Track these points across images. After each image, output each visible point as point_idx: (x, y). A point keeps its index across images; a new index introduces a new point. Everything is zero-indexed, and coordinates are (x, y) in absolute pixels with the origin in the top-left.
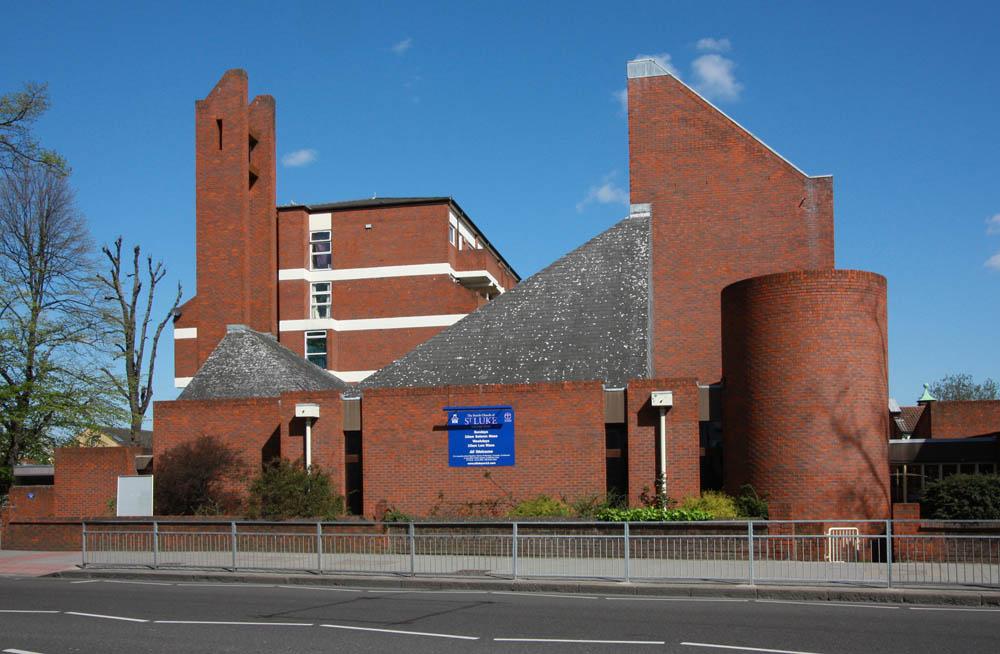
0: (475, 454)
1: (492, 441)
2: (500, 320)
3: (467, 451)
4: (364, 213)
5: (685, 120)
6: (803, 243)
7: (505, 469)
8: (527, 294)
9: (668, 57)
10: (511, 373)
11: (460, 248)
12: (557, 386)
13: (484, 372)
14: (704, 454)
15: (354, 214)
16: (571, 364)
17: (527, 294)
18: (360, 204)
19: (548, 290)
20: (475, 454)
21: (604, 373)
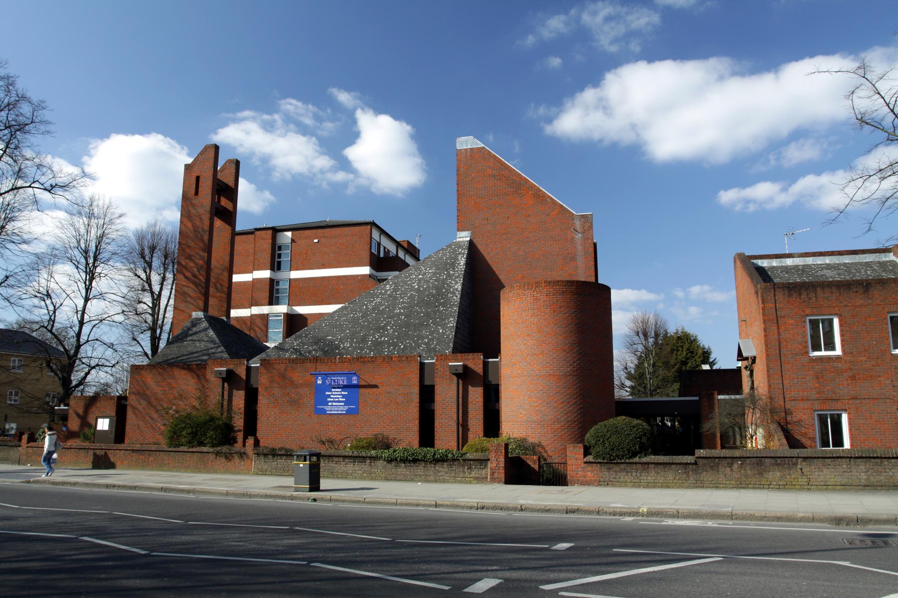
1: (344, 396)
2: (361, 311)
3: (326, 404)
4: (313, 231)
5: (494, 176)
6: (573, 259)
9: (408, 128)
10: (362, 349)
11: (382, 255)
15: (307, 232)
17: (380, 294)
19: (395, 290)
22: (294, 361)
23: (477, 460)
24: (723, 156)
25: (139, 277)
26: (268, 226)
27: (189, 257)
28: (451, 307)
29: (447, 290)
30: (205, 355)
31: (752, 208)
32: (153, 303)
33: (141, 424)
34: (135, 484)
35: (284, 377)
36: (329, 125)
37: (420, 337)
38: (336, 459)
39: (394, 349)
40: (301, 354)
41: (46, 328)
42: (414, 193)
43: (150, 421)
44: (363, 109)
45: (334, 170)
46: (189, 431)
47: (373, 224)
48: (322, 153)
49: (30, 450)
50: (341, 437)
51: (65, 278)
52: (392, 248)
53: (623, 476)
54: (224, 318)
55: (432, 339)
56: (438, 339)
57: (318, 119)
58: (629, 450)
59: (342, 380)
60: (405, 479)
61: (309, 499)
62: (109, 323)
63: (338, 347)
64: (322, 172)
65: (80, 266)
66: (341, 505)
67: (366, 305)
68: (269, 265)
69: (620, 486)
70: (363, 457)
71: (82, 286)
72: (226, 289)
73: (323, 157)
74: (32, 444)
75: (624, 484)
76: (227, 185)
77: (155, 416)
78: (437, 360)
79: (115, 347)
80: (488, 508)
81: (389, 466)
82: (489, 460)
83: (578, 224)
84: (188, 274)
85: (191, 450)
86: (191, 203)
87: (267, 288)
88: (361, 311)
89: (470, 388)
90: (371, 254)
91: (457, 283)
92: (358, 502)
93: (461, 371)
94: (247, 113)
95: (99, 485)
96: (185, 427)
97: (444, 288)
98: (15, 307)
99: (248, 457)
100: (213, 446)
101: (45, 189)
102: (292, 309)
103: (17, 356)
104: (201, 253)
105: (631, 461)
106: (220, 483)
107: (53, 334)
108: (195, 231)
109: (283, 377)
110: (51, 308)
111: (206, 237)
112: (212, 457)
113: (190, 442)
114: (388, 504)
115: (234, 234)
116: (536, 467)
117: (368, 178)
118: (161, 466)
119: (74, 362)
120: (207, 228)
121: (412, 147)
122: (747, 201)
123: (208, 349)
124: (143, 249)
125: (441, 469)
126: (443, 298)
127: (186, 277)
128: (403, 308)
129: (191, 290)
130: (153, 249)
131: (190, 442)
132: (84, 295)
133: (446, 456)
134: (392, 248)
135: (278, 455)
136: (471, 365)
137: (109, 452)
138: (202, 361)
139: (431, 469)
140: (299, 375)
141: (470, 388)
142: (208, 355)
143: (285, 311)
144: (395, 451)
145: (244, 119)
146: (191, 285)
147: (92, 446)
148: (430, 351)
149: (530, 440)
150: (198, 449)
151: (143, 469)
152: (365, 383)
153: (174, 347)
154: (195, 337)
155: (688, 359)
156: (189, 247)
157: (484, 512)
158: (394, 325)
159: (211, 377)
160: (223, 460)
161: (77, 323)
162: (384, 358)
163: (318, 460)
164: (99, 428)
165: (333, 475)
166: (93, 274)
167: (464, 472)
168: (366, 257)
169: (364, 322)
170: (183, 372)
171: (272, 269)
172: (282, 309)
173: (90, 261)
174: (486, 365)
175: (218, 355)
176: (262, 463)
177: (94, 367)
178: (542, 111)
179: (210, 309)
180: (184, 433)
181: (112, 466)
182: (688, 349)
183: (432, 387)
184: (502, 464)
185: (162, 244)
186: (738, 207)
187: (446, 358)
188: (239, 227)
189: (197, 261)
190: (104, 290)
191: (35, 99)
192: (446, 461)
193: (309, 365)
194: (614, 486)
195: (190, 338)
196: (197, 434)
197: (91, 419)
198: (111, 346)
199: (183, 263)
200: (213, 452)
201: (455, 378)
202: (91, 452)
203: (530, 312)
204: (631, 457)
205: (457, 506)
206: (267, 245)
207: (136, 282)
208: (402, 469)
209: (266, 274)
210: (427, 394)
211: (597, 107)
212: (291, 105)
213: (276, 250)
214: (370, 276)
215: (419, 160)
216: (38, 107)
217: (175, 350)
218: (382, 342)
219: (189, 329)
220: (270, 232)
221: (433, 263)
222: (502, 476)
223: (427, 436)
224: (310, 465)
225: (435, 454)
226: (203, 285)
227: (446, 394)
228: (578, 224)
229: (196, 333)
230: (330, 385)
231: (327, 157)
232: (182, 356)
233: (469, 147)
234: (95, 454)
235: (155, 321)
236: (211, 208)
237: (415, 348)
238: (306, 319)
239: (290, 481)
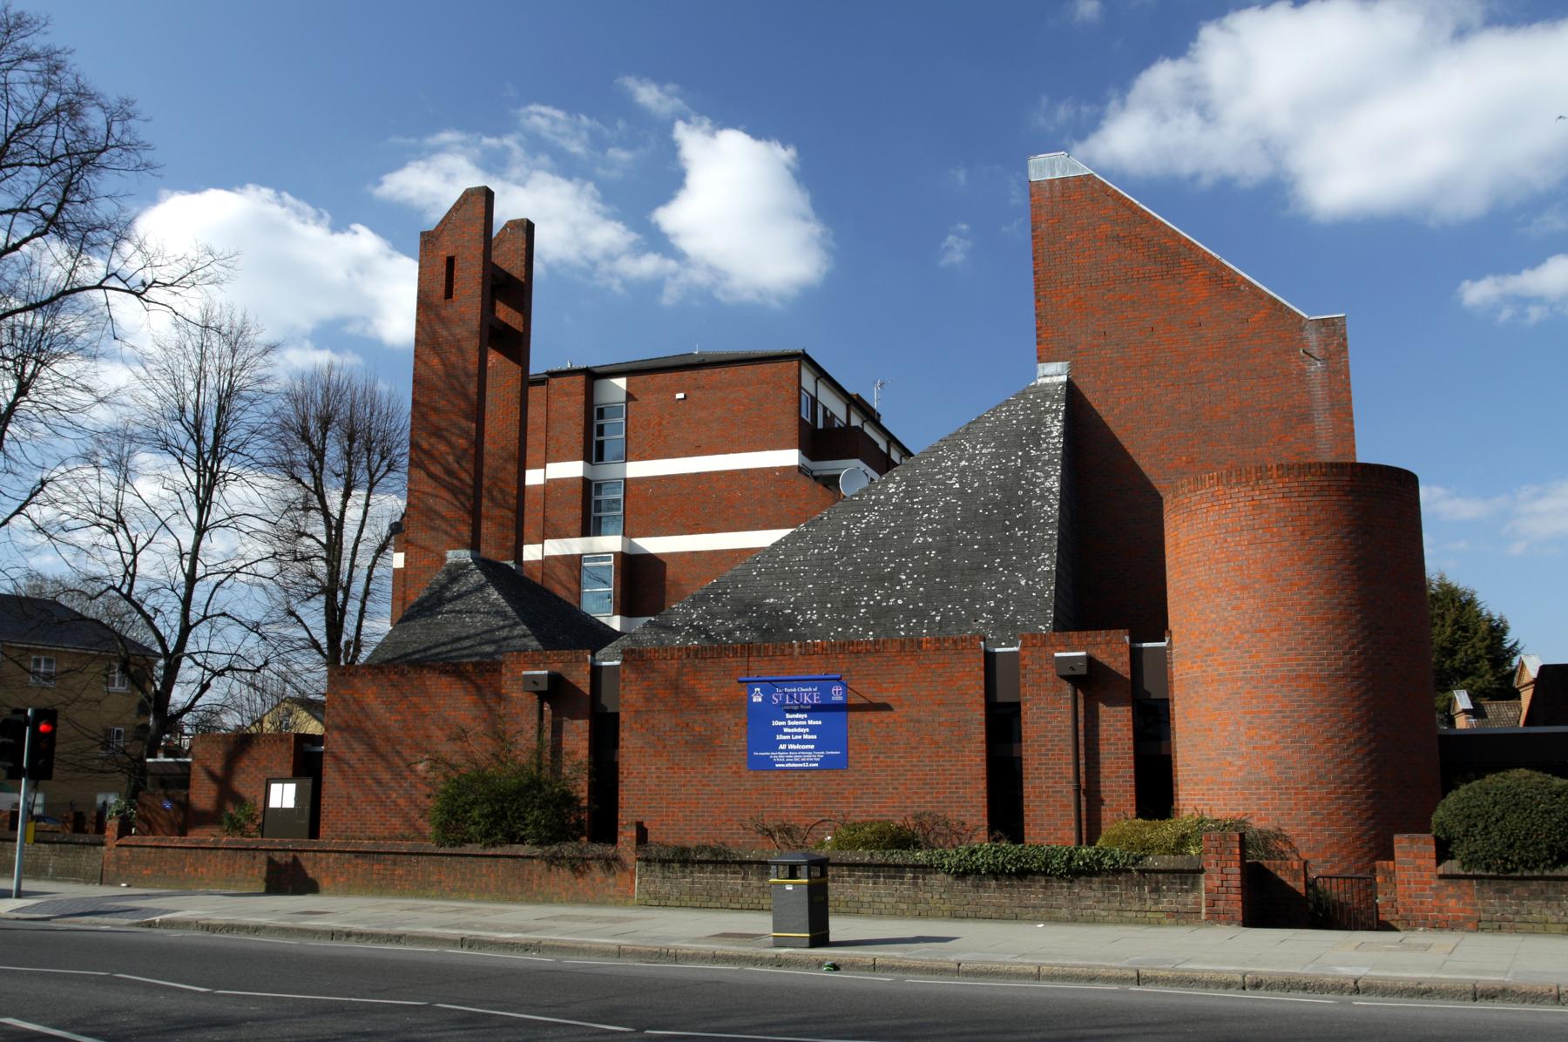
0: (787, 750)
1: (813, 729)
2: (835, 541)
3: (774, 746)
4: (674, 375)
5: (1117, 238)
6: (1305, 417)
10: (847, 624)
11: (820, 425)
12: (913, 645)
13: (805, 623)
14: (1015, 745)
15: (660, 377)
16: (937, 610)
17: (876, 502)
18: (645, 365)
19: (909, 494)
20: (787, 750)
21: (987, 624)
22: (697, 653)
23: (1174, 871)
24: (1470, 203)
25: (299, 481)
26: (576, 366)
27: (437, 433)
28: (1042, 528)
29: (1026, 492)
30: (488, 642)
31: (1535, 313)
32: (329, 536)
33: (356, 794)
34: (401, 929)
35: (677, 688)
36: (621, 155)
37: (977, 596)
39: (920, 623)
40: (709, 637)
41: (119, 590)
42: (808, 299)
43: (376, 788)
44: (687, 121)
45: (638, 250)
46: (487, 809)
47: (803, 358)
48: (608, 217)
49: (126, 852)
50: (809, 820)
51: (158, 483)
52: (838, 408)
53: (1537, 910)
54: (511, 563)
55: (1005, 601)
56: (1017, 601)
57: (599, 143)
58: (1550, 848)
59: (810, 695)
60: (1000, 916)
61: (820, 965)
62: (229, 583)
63: (791, 621)
64: (610, 257)
65: (185, 459)
66: (912, 980)
67: (847, 528)
68: (580, 449)
69: (1532, 932)
70: (897, 866)
71: (189, 498)
72: (513, 501)
73: (613, 223)
74: (126, 840)
75: (1541, 928)
76: (508, 276)
77: (386, 777)
78: (1024, 647)
79: (262, 629)
80: (1271, 986)
81: (960, 885)
82: (1202, 871)
83: (1313, 340)
84: (436, 469)
85: (491, 851)
86: (438, 315)
87: (579, 497)
88: (835, 541)
89: (1102, 707)
90: (801, 420)
91: (1048, 476)
92: (943, 971)
93: (1082, 670)
94: (446, 137)
95: (314, 933)
96: (474, 803)
97: (1021, 487)
98: (60, 546)
99: (624, 868)
100: (540, 844)
101: (130, 292)
102: (632, 545)
103: (39, 652)
104: (464, 423)
105: (1557, 872)
106: (590, 925)
107: (133, 603)
108: (448, 375)
109: (676, 688)
110: (126, 547)
111: (472, 389)
112: (539, 867)
113: (487, 835)
114: (1018, 976)
115: (527, 382)
116: (1300, 886)
117: (711, 269)
118: (422, 888)
119: (179, 661)
120: (473, 368)
121: (799, 200)
122: (1523, 301)
123: (492, 631)
124: (305, 419)
125: (1085, 893)
126: (1020, 510)
127: (430, 475)
128: (932, 533)
129: (443, 503)
130: (325, 422)
131: (487, 835)
132: (194, 519)
133: (1099, 862)
134: (838, 408)
135: (694, 863)
136: (1102, 657)
137: (302, 857)
138: (483, 655)
139: (1062, 893)
140: (712, 684)
141: (1102, 707)
142: (495, 642)
144: (973, 852)
145: (441, 149)
146: (448, 496)
147: (265, 843)
148: (1006, 628)
149: (1256, 824)
151: (381, 894)
152: (861, 701)
153: (417, 626)
154: (459, 605)
155: (1456, 643)
156: (435, 409)
157: (1261, 995)
158: (913, 571)
159: (514, 691)
160: (566, 873)
161: (182, 578)
162: (903, 644)
163: (824, 874)
164: (274, 803)
165: (855, 910)
166: (213, 476)
167: (1141, 899)
168: (790, 427)
169: (845, 565)
170: (445, 680)
171: (587, 458)
172: (611, 543)
173: (208, 446)
174: (1136, 656)
175: (517, 643)
176: (657, 881)
177: (221, 673)
178: (1063, 112)
179: (483, 546)
180: (475, 813)
181: (311, 887)
182: (1456, 622)
183: (1015, 709)
184: (1235, 881)
185: (344, 412)
186: (1506, 314)
187: (1045, 641)
188: (537, 367)
189: (454, 439)
190: (237, 509)
191: (112, 99)
192: (1098, 874)
193: (732, 661)
194: (1515, 930)
195: (448, 607)
196: (504, 817)
197: (244, 784)
198: (255, 627)
199: (425, 445)
200: (542, 857)
201: (1067, 688)
202: (263, 857)
203: (1246, 536)
204: (1555, 865)
205: (1191, 982)
206: (576, 407)
207: (293, 493)
208: (992, 894)
209: (574, 469)
210: (1003, 724)
211: (1186, 104)
212: (542, 117)
213: (593, 415)
214: (800, 469)
215: (816, 229)
216: (122, 112)
217: (419, 635)
218: (889, 609)
219: (444, 587)
220: (581, 379)
221: (990, 433)
222: (1237, 908)
223: (1006, 812)
224: (810, 886)
225: (1071, 859)
226: (469, 491)
227: (1048, 722)
228: (1313, 340)
229: (460, 596)
230: (782, 704)
231: (620, 226)
232: (436, 646)
233: (1058, 175)
234: (270, 861)
235: (334, 573)
236: (481, 325)
237: (967, 622)
238: (664, 564)
239: (762, 923)
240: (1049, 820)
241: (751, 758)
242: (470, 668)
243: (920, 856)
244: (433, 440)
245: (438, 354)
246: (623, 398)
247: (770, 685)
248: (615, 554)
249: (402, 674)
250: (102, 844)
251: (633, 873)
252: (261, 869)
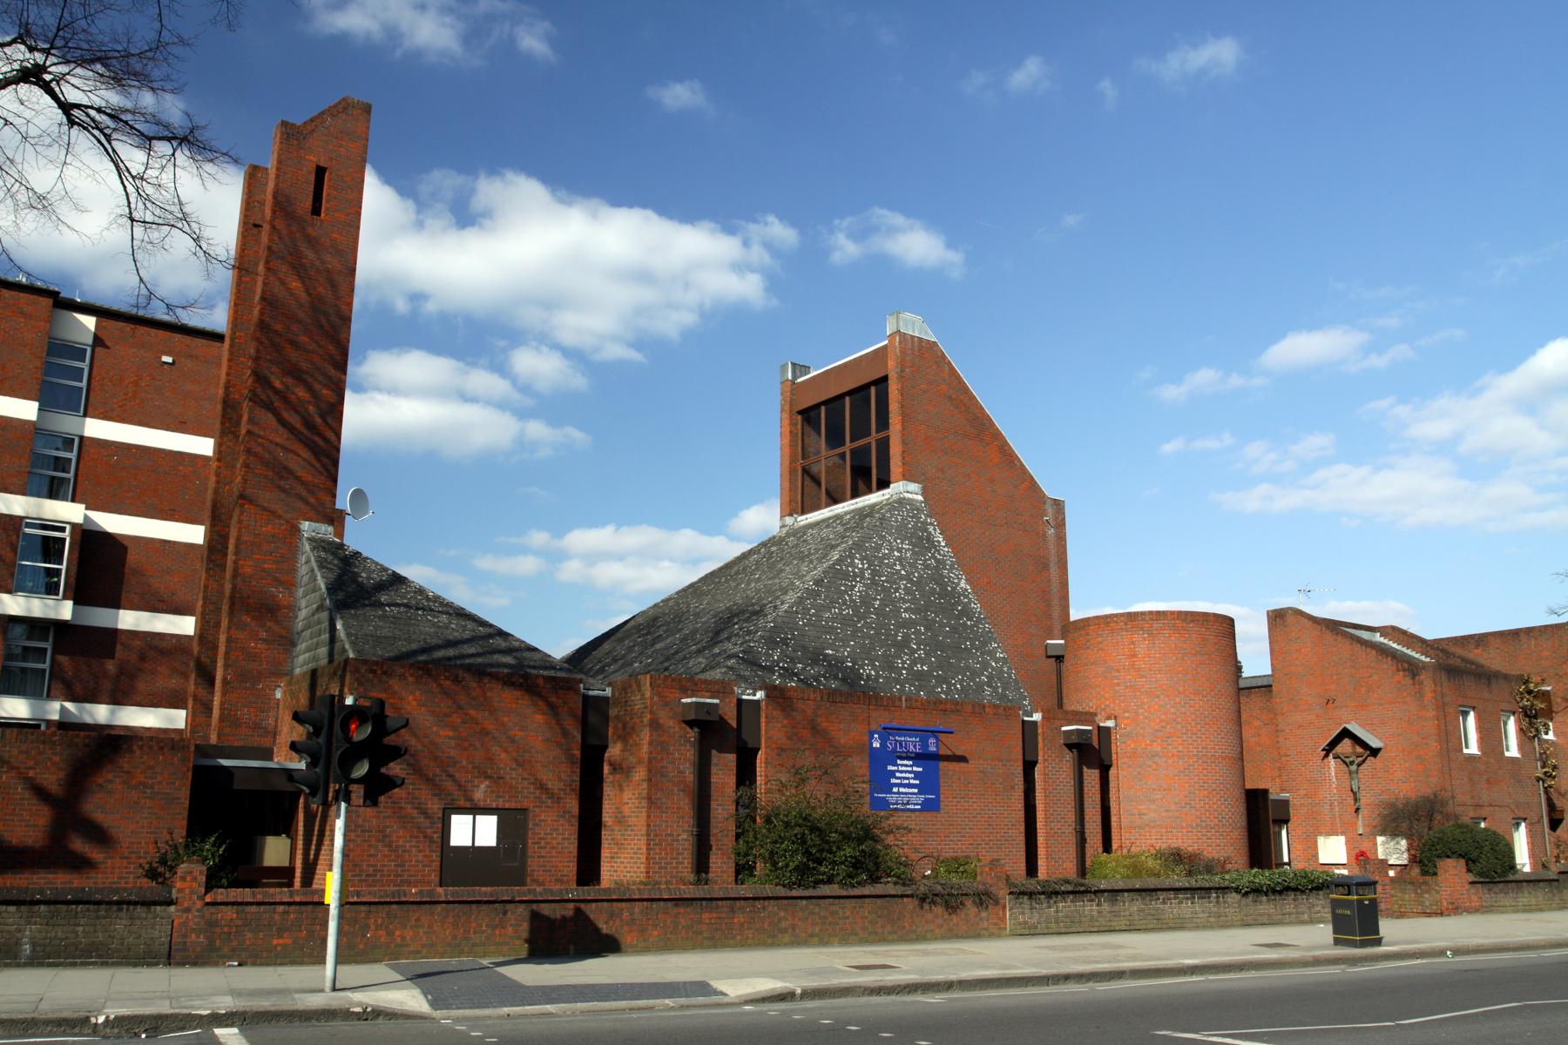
5: (950, 398)
6: (1046, 567)
7: (928, 816)
8: (855, 575)
22: (832, 696)
38: (1162, 895)
53: (1506, 900)
59: (913, 743)
84: (294, 420)
99: (997, 903)
109: (814, 729)
143: (79, 519)
146: (306, 454)
150: (867, 890)
156: (292, 343)
189: (317, 387)
208: (1265, 906)
230: (894, 750)
234: (536, 917)
238: (125, 548)
240: (1055, 861)
241: (874, 799)
242: (541, 682)
243: (1217, 880)
244: (290, 381)
245: (301, 278)
246: (90, 341)
247: (887, 732)
248: (74, 526)
249: (456, 680)
250: (170, 903)
251: (1004, 907)
252: (517, 925)
